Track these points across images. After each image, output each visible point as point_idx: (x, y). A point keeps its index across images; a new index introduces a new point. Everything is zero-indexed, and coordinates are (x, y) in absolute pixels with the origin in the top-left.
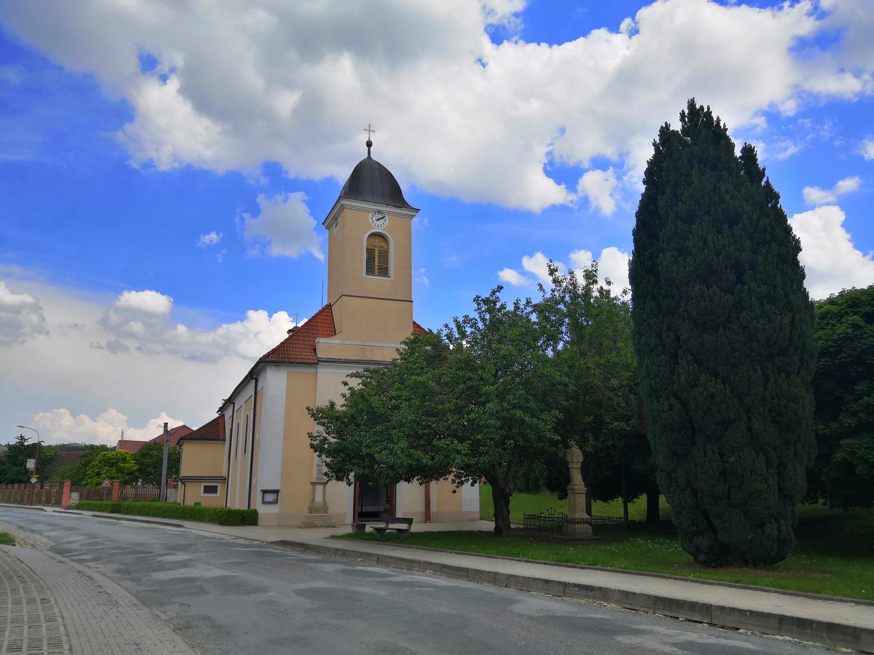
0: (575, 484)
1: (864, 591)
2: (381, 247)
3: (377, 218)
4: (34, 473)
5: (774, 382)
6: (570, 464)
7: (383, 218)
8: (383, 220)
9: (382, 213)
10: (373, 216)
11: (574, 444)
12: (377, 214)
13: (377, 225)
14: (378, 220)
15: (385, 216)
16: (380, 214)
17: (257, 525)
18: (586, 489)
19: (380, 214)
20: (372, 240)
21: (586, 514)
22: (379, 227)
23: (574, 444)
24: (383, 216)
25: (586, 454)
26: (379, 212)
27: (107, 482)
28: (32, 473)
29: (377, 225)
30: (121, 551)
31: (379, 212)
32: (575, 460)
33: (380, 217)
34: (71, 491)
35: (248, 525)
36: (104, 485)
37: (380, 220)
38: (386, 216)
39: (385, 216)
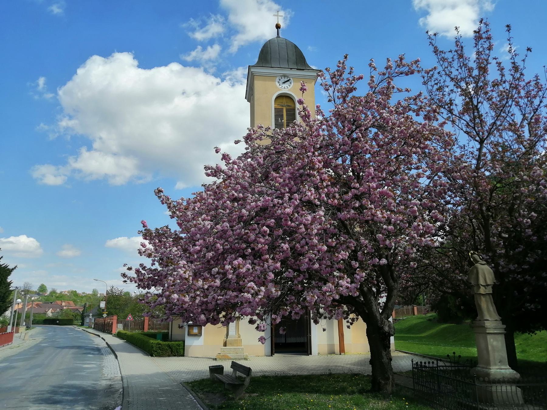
0: (485, 318)
1: (537, 300)
2: (288, 106)
3: (284, 81)
4: (105, 310)
5: (527, 346)
6: (475, 288)
7: (288, 81)
8: (289, 82)
9: (288, 77)
10: (280, 80)
11: (479, 260)
12: (283, 78)
13: (283, 87)
14: (284, 83)
15: (290, 79)
16: (286, 78)
17: (183, 355)
18: (505, 326)
19: (286, 78)
20: (280, 100)
21: (508, 367)
22: (286, 89)
23: (479, 260)
24: (288, 79)
25: (497, 274)
26: (285, 76)
27: (130, 317)
28: (103, 310)
29: (283, 87)
30: (80, 373)
31: (285, 76)
32: (482, 282)
33: (286, 80)
34: (118, 323)
35: (175, 356)
36: (128, 319)
37: (286, 83)
38: (291, 79)
39: (290, 79)
